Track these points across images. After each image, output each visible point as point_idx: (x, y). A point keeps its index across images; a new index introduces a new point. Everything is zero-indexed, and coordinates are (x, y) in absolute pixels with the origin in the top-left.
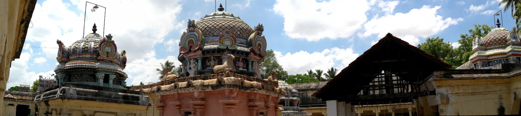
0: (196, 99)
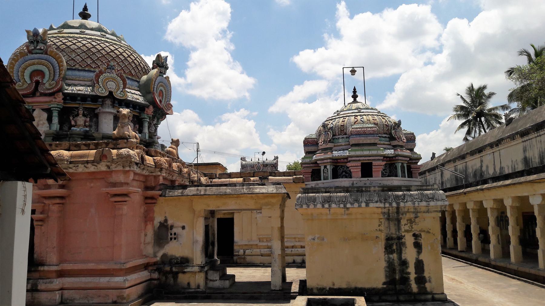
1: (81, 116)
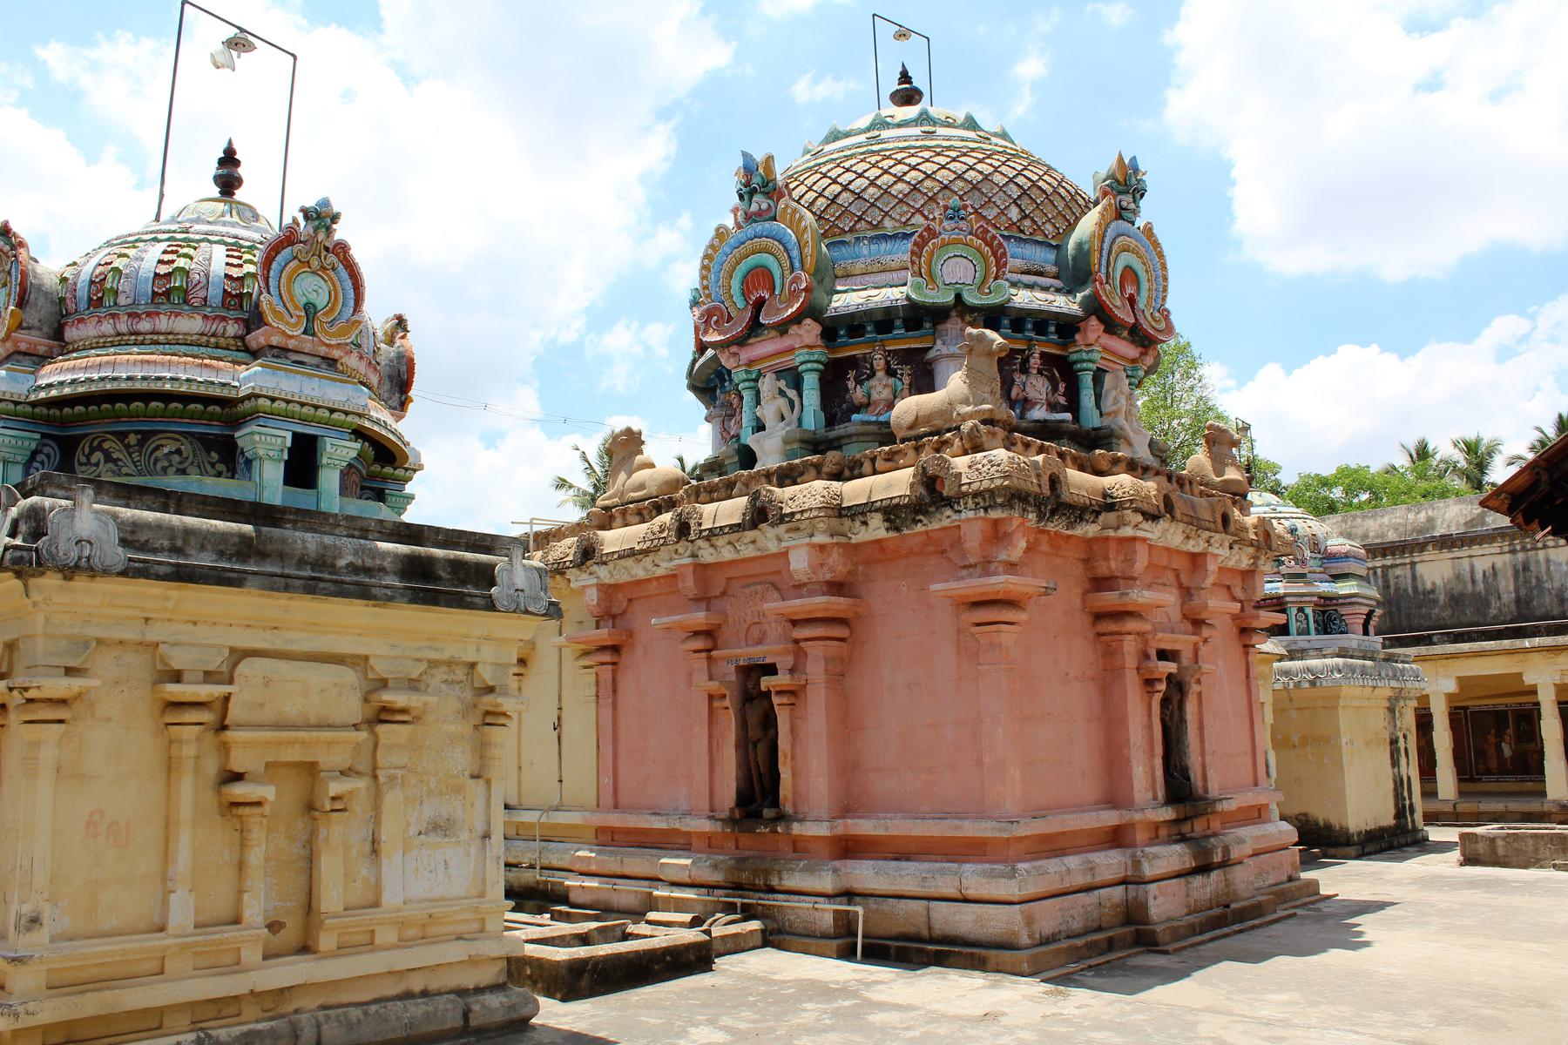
0: (799, 588)
1: (880, 374)
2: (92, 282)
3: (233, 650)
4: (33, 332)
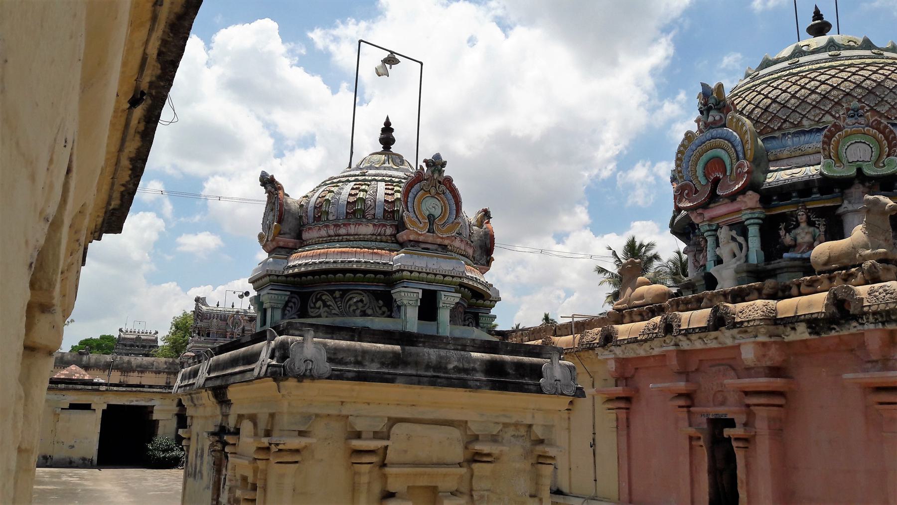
0: (749, 371)
1: (803, 225)
2: (315, 208)
3: (389, 419)
4: (287, 236)
